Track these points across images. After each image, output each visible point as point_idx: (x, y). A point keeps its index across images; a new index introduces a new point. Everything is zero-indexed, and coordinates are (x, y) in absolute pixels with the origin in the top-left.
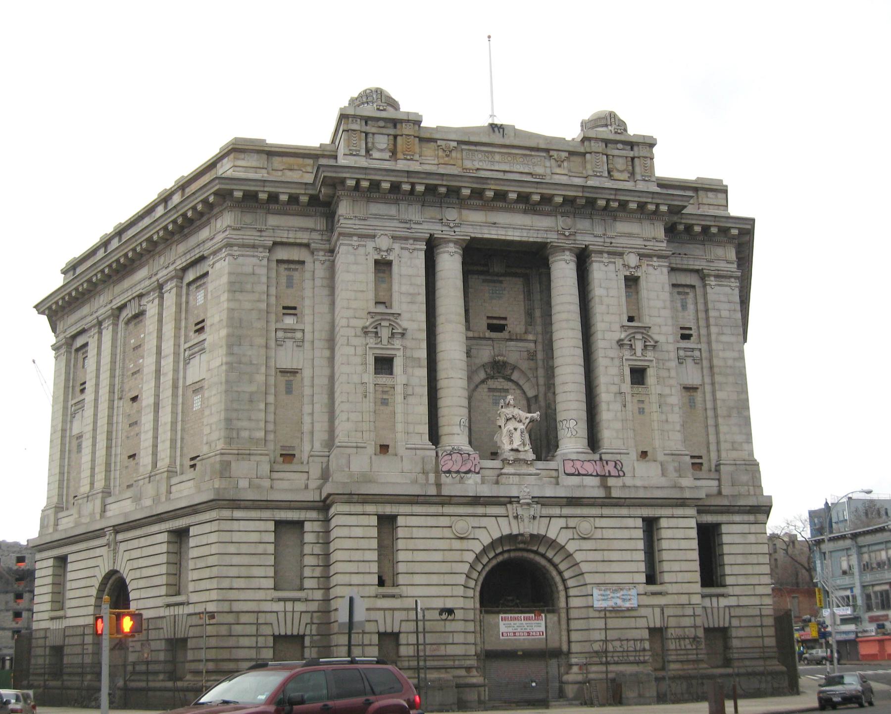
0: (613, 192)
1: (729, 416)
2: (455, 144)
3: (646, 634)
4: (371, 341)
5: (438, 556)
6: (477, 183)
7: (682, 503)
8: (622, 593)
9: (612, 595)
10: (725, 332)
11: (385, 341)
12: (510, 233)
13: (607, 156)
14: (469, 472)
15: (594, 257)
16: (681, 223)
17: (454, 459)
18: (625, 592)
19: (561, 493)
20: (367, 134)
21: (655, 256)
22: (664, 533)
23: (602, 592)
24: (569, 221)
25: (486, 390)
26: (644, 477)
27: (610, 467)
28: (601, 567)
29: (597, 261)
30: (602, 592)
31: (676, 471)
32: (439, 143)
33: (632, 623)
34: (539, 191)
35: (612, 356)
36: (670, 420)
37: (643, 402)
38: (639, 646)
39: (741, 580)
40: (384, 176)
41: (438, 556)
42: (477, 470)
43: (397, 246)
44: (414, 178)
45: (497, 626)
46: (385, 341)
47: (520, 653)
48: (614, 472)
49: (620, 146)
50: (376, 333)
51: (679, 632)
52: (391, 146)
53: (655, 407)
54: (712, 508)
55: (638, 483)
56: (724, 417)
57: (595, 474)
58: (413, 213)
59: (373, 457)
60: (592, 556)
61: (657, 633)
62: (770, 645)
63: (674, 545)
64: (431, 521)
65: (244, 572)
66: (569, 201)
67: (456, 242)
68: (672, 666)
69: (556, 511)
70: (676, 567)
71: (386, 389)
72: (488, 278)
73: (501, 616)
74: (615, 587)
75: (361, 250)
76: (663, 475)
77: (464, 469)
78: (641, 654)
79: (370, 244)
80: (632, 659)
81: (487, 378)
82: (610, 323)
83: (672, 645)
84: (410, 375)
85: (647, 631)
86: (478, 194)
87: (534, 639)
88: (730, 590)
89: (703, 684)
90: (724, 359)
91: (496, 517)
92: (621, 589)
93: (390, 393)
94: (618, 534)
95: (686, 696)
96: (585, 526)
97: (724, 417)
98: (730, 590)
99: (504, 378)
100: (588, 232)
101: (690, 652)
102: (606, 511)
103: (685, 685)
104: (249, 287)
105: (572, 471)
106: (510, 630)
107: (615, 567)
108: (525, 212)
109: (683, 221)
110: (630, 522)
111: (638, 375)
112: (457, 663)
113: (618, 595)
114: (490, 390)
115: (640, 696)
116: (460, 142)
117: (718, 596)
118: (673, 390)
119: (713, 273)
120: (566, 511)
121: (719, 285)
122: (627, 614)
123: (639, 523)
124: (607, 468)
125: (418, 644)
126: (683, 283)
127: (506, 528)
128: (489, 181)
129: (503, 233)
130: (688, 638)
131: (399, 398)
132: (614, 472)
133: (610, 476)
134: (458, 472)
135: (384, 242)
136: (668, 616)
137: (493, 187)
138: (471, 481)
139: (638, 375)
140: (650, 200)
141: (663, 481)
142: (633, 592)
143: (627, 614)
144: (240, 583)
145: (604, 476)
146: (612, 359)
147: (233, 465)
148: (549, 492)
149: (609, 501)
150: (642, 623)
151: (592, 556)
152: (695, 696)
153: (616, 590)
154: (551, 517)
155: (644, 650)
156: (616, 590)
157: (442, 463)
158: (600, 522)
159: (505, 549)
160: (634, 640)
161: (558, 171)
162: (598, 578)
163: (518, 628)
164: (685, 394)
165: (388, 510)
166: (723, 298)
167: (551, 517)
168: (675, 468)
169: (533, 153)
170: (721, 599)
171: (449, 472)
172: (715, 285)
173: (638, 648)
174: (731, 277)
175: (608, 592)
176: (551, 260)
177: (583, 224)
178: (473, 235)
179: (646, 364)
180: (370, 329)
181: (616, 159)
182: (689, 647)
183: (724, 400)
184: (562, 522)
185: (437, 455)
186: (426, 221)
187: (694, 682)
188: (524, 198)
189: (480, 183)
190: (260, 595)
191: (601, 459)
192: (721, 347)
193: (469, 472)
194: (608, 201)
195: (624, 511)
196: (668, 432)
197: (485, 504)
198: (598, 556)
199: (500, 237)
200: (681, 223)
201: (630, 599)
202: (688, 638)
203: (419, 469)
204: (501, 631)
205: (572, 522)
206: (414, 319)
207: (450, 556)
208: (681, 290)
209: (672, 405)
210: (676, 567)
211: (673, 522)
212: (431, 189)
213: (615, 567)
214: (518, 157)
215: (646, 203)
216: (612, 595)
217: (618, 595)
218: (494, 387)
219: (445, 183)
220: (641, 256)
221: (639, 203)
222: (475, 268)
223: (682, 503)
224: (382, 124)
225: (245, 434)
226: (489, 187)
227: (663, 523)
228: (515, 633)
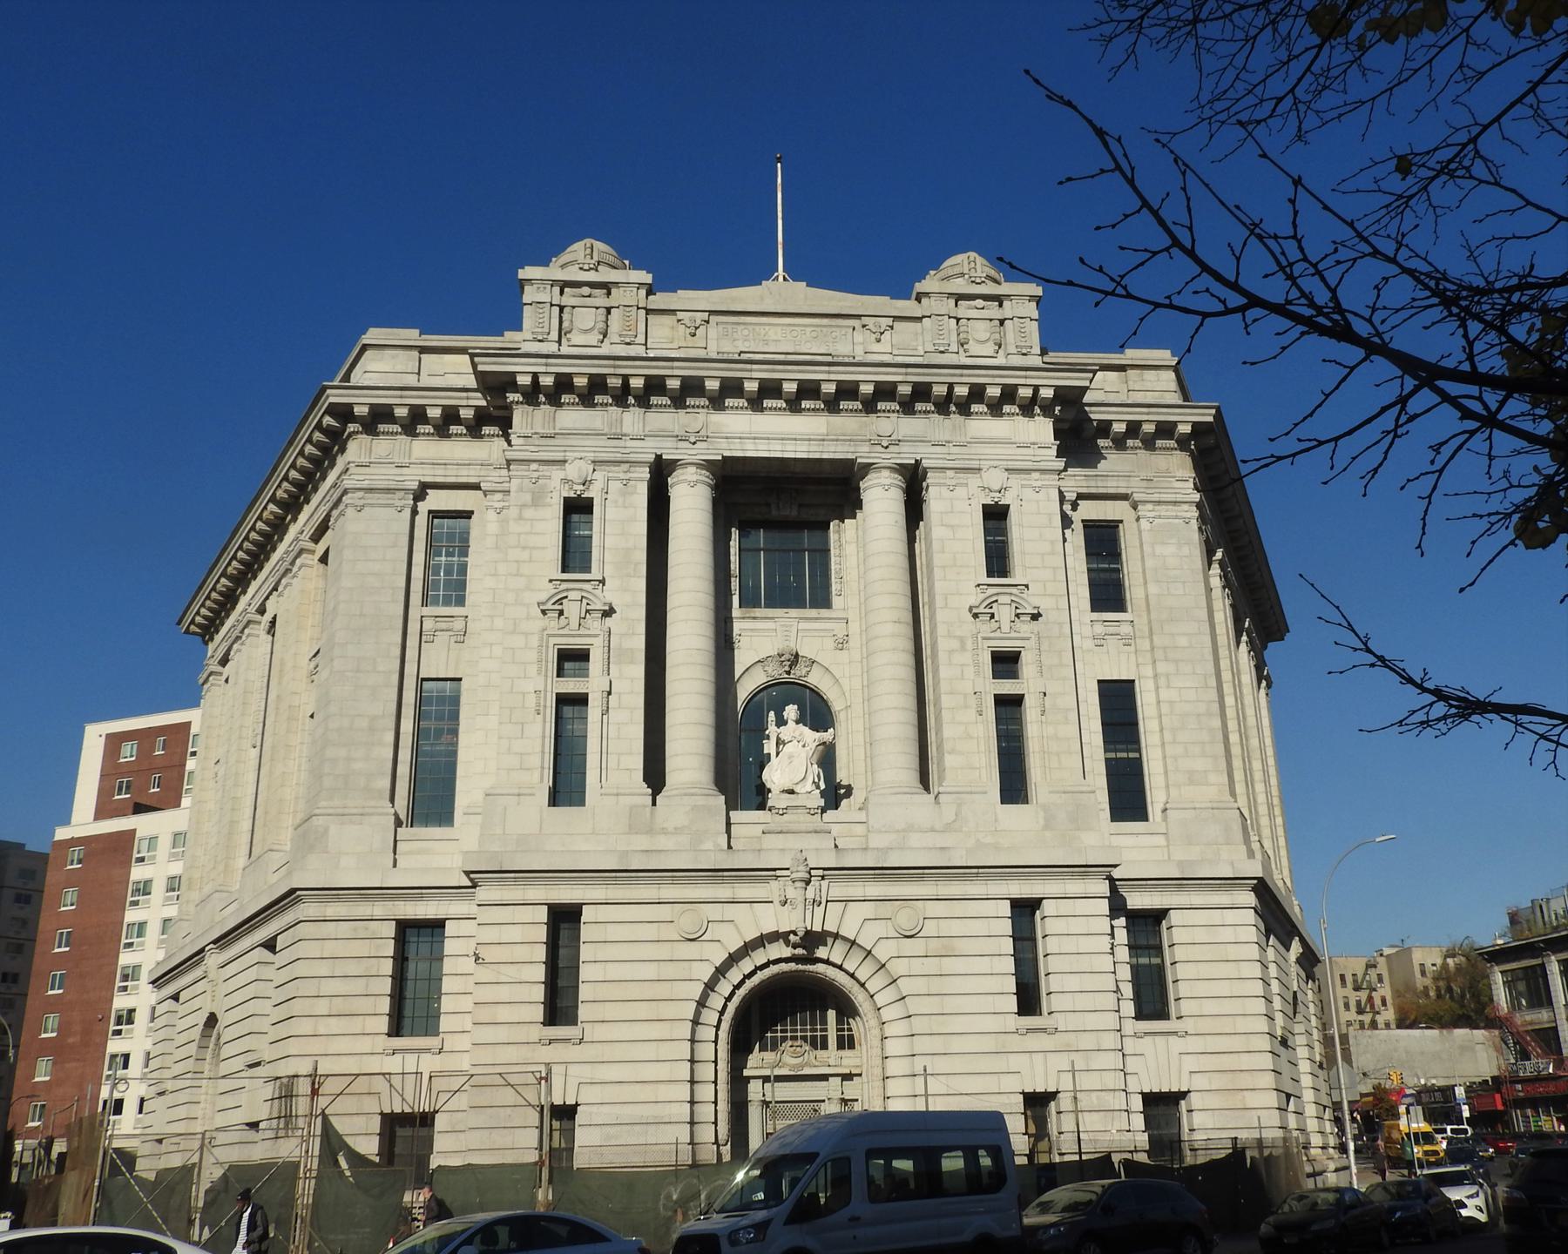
4: (552, 623)
11: (1006, 627)
12: (789, 448)
13: (958, 320)
15: (931, 478)
20: (562, 308)
22: (1052, 926)
28: (936, 985)
39: (1210, 1007)
41: (650, 971)
46: (1006, 627)
50: (561, 613)
52: (602, 325)
58: (632, 419)
60: (918, 966)
63: (1069, 945)
65: (339, 1005)
70: (1073, 983)
75: (960, 492)
79: (973, 481)
88: (1188, 1025)
96: (905, 918)
98: (1188, 1025)
100: (918, 436)
125: (1076, 1112)
135: (995, 478)
144: (335, 1025)
147: (333, 830)
151: (918, 966)
161: (876, 347)
165: (565, 894)
170: (425, 1057)
176: (862, 485)
178: (727, 454)
180: (981, 610)
184: (868, 909)
186: (654, 430)
188: (809, 390)
190: (365, 1045)
207: (668, 971)
210: (1073, 983)
224: (586, 290)
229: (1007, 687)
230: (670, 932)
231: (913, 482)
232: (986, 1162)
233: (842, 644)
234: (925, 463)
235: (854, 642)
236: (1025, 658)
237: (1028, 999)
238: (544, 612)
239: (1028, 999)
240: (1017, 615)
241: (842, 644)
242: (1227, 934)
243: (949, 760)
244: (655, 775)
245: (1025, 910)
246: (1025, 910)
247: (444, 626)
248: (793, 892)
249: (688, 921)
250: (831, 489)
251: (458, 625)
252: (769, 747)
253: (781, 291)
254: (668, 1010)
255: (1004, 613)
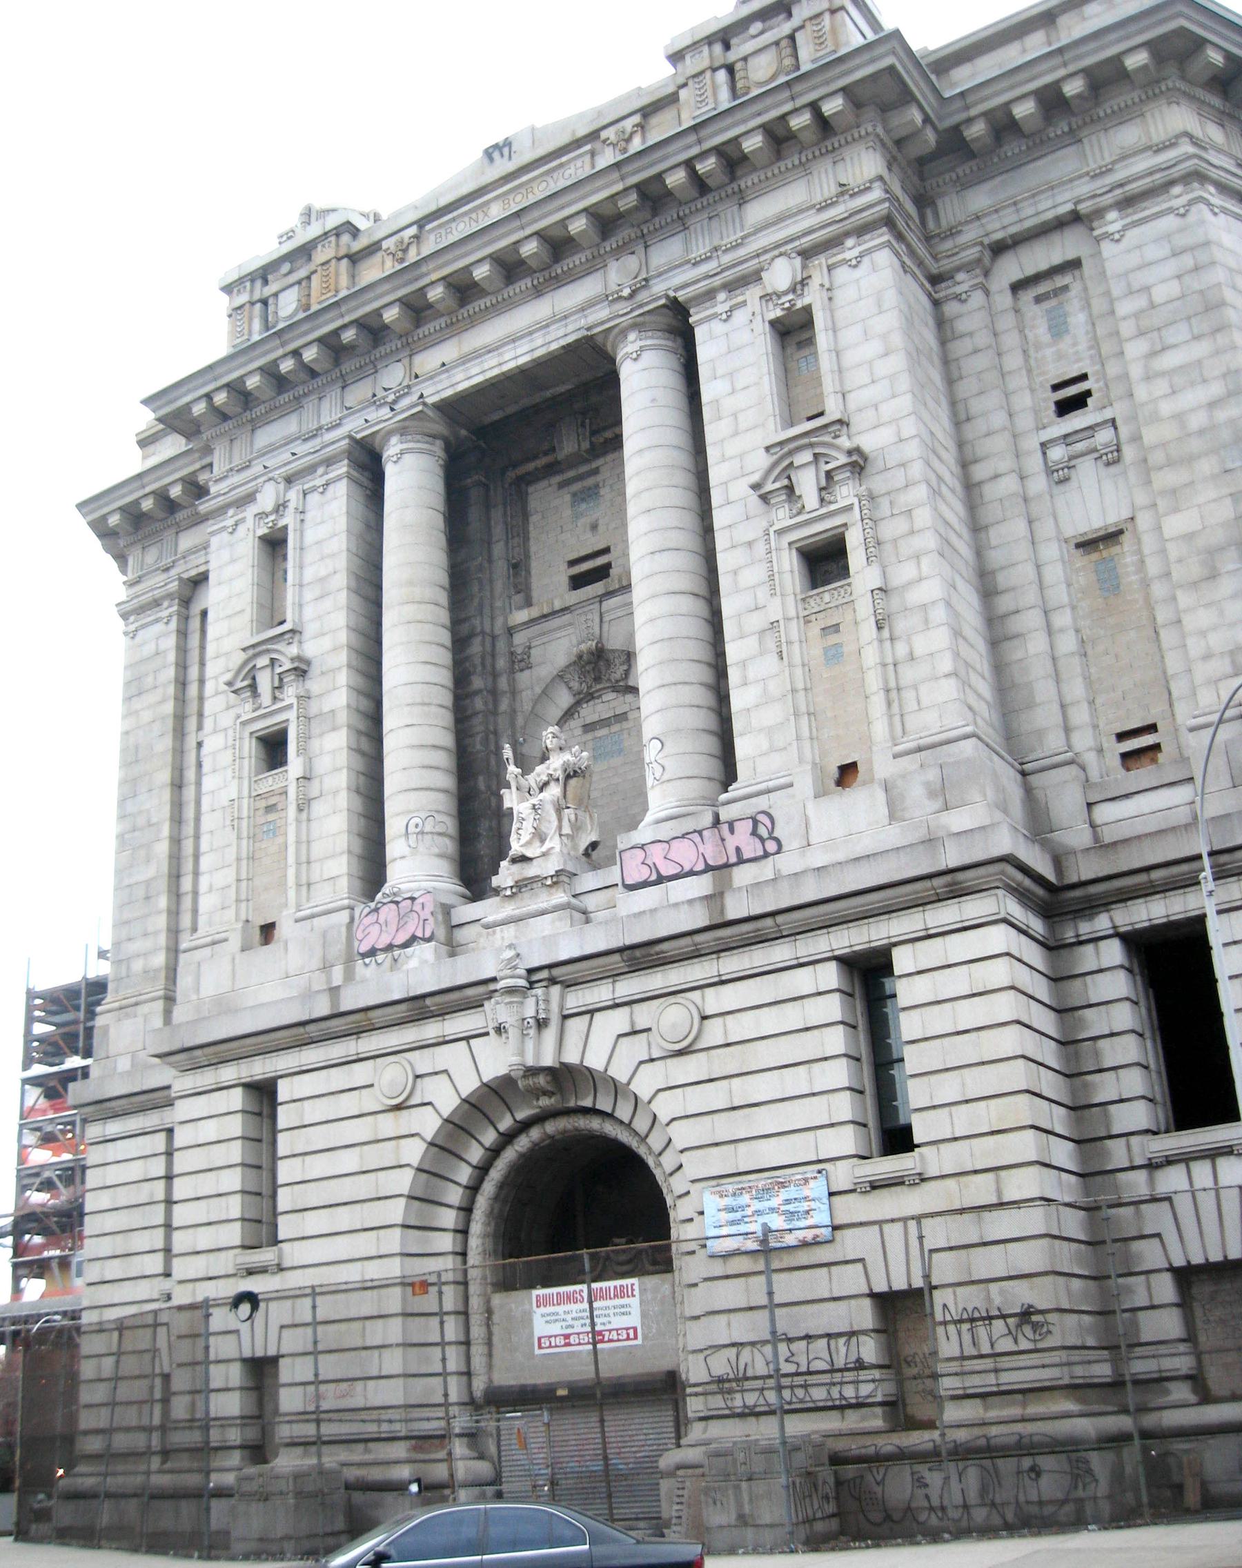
0: (692, 138)
1: (1213, 576)
2: (413, 230)
3: (865, 1315)
4: (782, 516)
5: (348, 1161)
6: (405, 285)
7: (951, 884)
8: (784, 1194)
9: (757, 1205)
10: (1172, 340)
14: (412, 940)
16: (970, 121)
17: (381, 920)
18: (791, 1192)
19: (597, 940)
21: (847, 234)
23: (728, 1201)
24: (631, 262)
25: (579, 731)
26: (836, 840)
27: (742, 838)
28: (725, 1127)
29: (701, 322)
30: (728, 1201)
31: (932, 794)
32: (385, 245)
33: (818, 1283)
34: (528, 231)
35: (750, 537)
36: (918, 651)
37: (836, 628)
38: (842, 1353)
40: (245, 364)
41: (348, 1161)
42: (427, 935)
43: (293, 495)
44: (292, 340)
45: (527, 1320)
47: (562, 1392)
48: (751, 848)
49: (757, 27)
51: (970, 1299)
53: (868, 630)
54: (1156, 875)
55: (818, 858)
56: (1194, 585)
57: (700, 866)
59: (238, 957)
61: (899, 1309)
62: (400, 1360)
63: (939, 1020)
64: (338, 1078)
66: (606, 222)
67: (402, 430)
68: (953, 1413)
69: (601, 993)
71: (272, 801)
72: (571, 474)
73: (535, 1292)
74: (761, 1181)
76: (892, 817)
77: (401, 938)
78: (849, 1376)
79: (752, 294)
80: (819, 1394)
81: (578, 703)
82: (741, 456)
83: (948, 1344)
84: (328, 754)
85: (867, 1303)
86: (417, 309)
87: (616, 1350)
89: (1036, 1471)
90: (1180, 417)
91: (467, 1039)
92: (782, 1185)
93: (280, 807)
94: (770, 1021)
95: (979, 1515)
96: (672, 1019)
97: (1194, 585)
99: (615, 689)
100: (674, 265)
101: (1005, 1362)
102: (732, 964)
103: (973, 1475)
104: (149, 680)
105: (644, 874)
106: (556, 1329)
107: (766, 1120)
108: (538, 292)
109: (973, 112)
110: (803, 981)
111: (824, 561)
112: (385, 1427)
113: (774, 1202)
114: (588, 728)
115: (743, 1520)
116: (421, 223)
117: (1213, 1154)
118: (925, 561)
119: (1108, 199)
120: (629, 987)
121: (1136, 224)
122: (803, 1257)
123: (830, 976)
124: (732, 842)
126: (1043, 266)
127: (496, 1060)
128: (424, 269)
129: (494, 362)
130: (1004, 1317)
131: (292, 811)
132: (751, 848)
133: (741, 861)
134: (390, 948)
136: (931, 1251)
137: (435, 276)
138: (413, 963)
139: (824, 561)
140: (788, 107)
141: (893, 836)
142: (818, 1188)
143: (803, 1257)
145: (727, 866)
146: (750, 544)
148: (571, 944)
149: (723, 935)
150: (851, 1280)
152: (1010, 1517)
153: (766, 1190)
154: (591, 1012)
155: (860, 1365)
156: (766, 1190)
157: (360, 935)
158: (714, 1000)
159: (521, 1115)
160: (829, 1336)
162: (717, 1162)
163: (572, 1322)
164: (1081, 560)
165: (259, 1069)
166: (1152, 252)
167: (591, 1012)
168: (927, 784)
169: (564, 159)
171: (372, 952)
172: (1125, 228)
173: (840, 1362)
174: (1172, 183)
175: (745, 1199)
177: (666, 252)
179: (837, 521)
180: (769, 487)
181: (753, 62)
182: (1006, 1345)
183: (1189, 537)
184: (618, 1021)
185: (352, 919)
187: (1006, 1466)
189: (410, 282)
191: (717, 822)
192: (1161, 387)
193: (412, 940)
194: (689, 164)
195: (780, 953)
196: (915, 687)
197: (443, 1013)
198: (715, 1096)
199: (489, 375)
200: (970, 121)
201: (806, 1208)
202: (1004, 1317)
203: (316, 963)
204: (537, 1334)
205: (644, 1015)
206: (325, 626)
208: (1043, 288)
209: (924, 607)
211: (931, 953)
212: (332, 345)
213: (766, 1120)
214: (534, 185)
215: (783, 118)
216: (757, 1205)
217: (774, 1202)
218: (595, 718)
219: (347, 319)
220: (806, 254)
221: (767, 129)
222: (531, 466)
223: (951, 884)
225: (138, 966)
226: (426, 281)
227: (902, 960)
228: (567, 1336)
230: (368, 1101)
232: (38, 1002)
234: (682, 295)
236: (854, 540)
238: (765, 498)
240: (829, 474)
244: (372, 870)
245: (869, 976)
246: (869, 976)
247: (1080, 447)
249: (390, 1077)
251: (1104, 436)
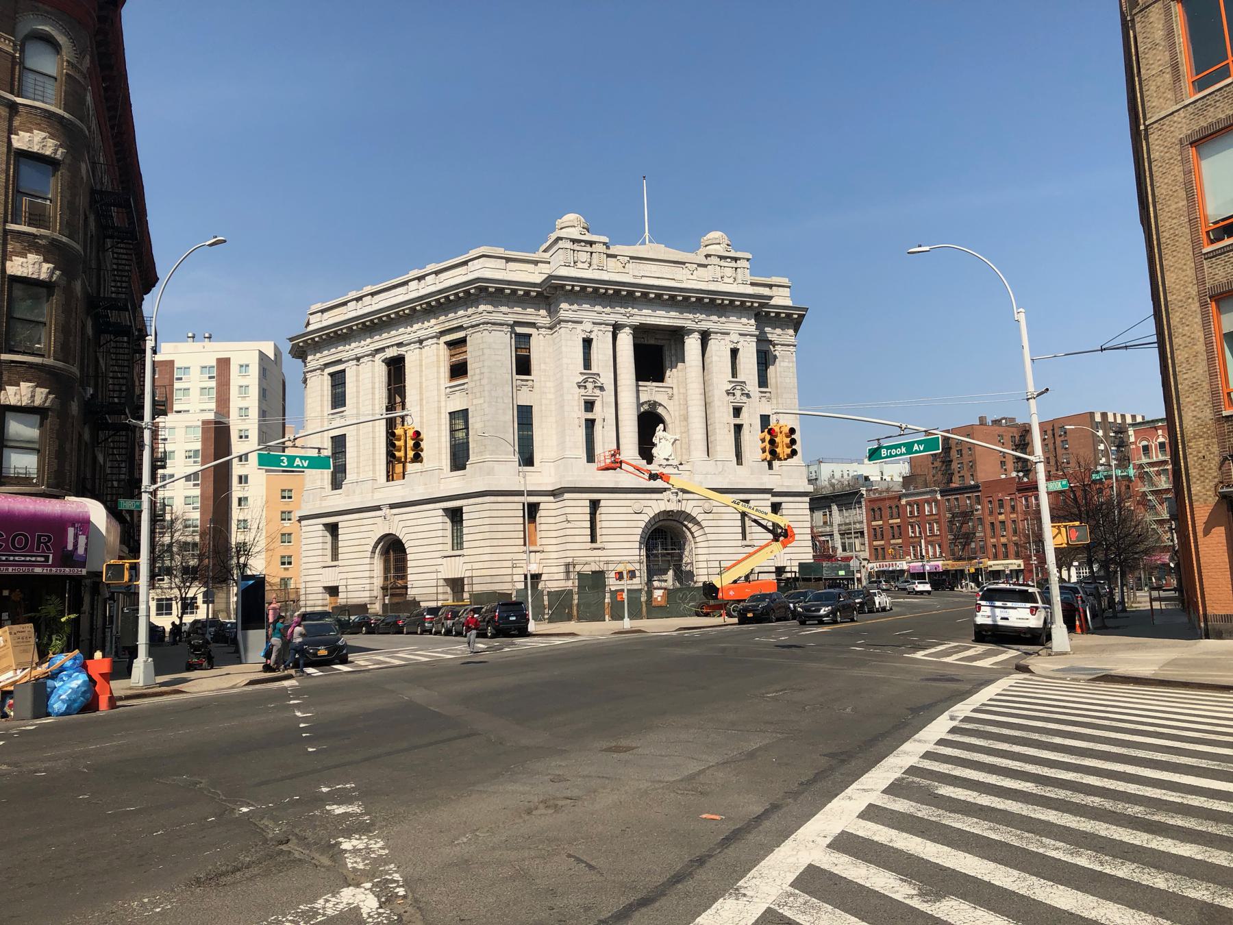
79: (726, 337)
100: (710, 322)
229: (590, 416)
231: (705, 337)
233: (671, 398)
235: (676, 397)
237: (593, 539)
239: (593, 539)
241: (671, 398)
242: (800, 512)
243: (718, 448)
245: (595, 505)
246: (595, 505)
248: (673, 497)
249: (637, 506)
250: (677, 335)
252: (655, 440)
253: (648, 245)
254: (365, 548)
255: (590, 386)
